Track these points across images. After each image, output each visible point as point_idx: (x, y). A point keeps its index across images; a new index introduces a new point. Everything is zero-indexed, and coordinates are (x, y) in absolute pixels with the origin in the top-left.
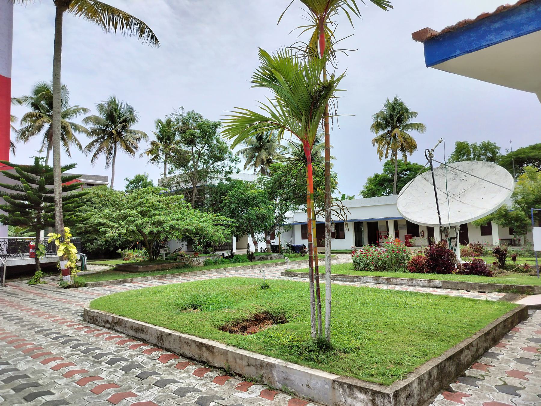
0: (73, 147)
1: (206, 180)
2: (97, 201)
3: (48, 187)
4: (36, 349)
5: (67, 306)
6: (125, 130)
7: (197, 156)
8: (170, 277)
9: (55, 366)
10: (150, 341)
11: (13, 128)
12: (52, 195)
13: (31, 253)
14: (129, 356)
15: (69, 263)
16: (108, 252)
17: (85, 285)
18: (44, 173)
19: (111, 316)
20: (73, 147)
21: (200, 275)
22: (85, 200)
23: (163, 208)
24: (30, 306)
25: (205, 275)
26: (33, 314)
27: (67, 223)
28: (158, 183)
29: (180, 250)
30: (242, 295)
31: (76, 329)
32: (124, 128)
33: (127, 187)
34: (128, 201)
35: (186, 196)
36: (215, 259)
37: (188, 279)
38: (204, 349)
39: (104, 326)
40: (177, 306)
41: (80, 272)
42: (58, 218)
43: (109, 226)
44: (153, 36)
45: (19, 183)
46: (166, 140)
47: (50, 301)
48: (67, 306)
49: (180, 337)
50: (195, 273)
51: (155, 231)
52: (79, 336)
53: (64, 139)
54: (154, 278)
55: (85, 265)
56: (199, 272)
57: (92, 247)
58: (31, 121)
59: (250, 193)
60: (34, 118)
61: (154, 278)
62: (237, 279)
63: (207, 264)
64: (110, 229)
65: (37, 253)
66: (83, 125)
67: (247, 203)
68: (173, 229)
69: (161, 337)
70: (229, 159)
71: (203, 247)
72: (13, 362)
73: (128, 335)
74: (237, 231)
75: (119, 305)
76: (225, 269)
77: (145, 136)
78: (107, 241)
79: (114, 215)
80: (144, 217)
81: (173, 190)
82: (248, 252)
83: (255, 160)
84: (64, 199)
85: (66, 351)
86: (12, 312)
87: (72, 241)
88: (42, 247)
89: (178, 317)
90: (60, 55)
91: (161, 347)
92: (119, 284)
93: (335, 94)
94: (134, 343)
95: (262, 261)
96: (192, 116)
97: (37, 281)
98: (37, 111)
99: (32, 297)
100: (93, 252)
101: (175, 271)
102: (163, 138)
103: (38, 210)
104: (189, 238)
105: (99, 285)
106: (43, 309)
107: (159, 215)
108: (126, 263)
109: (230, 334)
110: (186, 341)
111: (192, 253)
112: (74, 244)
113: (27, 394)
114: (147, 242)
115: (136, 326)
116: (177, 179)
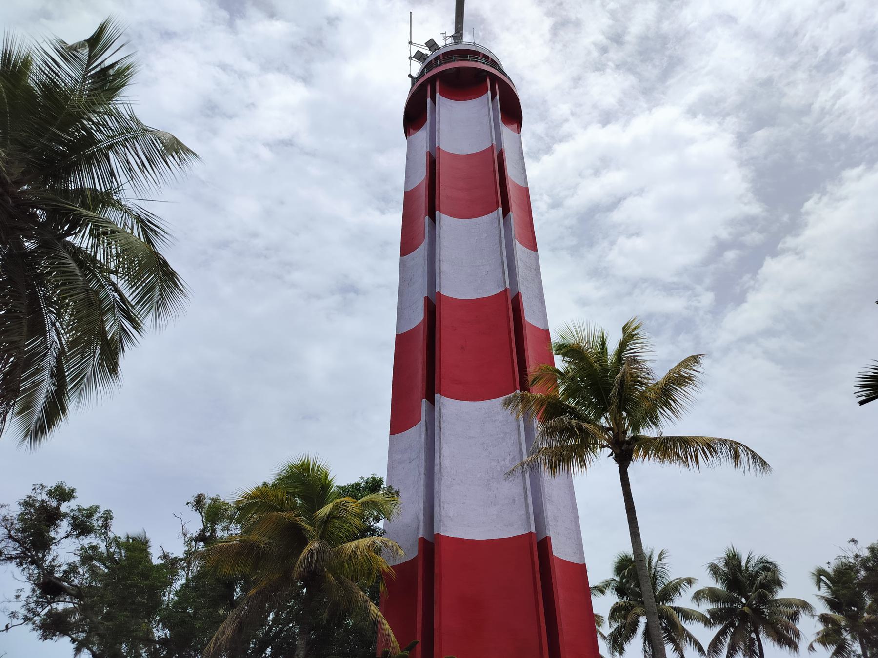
6: (764, 603)
11: (601, 634)
32: (763, 599)
44: (754, 455)
53: (672, 640)
77: (805, 606)
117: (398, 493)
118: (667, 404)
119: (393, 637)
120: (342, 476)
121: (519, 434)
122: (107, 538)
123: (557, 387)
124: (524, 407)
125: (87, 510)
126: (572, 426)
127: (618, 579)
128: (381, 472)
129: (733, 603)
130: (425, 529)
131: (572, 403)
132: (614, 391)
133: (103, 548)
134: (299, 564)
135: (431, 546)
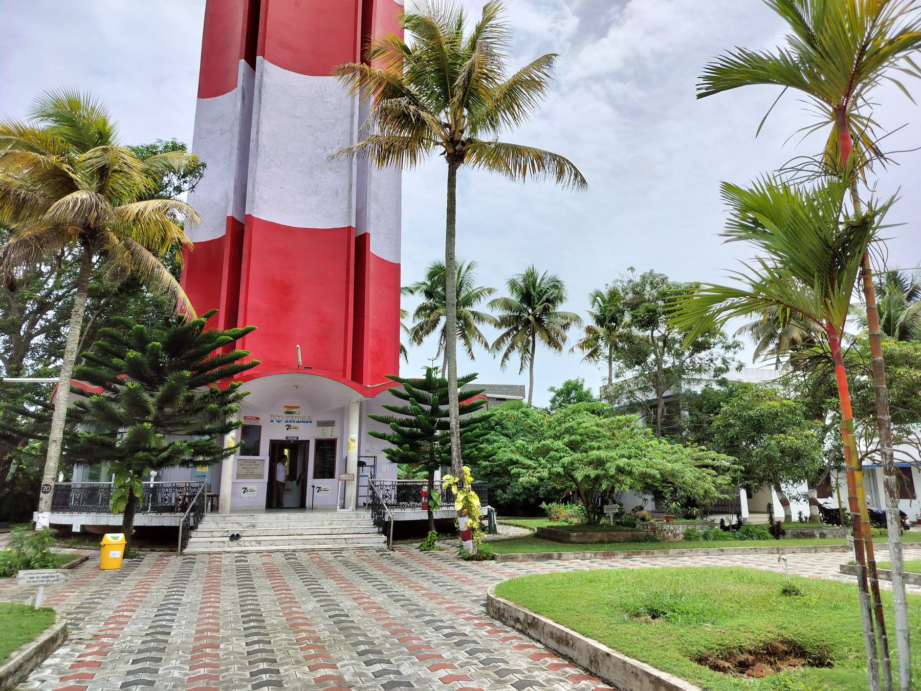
0: (477, 346)
1: (679, 386)
2: (510, 425)
3: (443, 408)
4: (424, 647)
5: (466, 587)
6: (546, 314)
7: (661, 344)
8: (622, 556)
10: (579, 662)
12: (447, 419)
15: (470, 521)
16: (526, 505)
17: (493, 558)
18: (438, 388)
20: (477, 346)
22: (493, 423)
23: (605, 436)
26: (423, 595)
27: (468, 460)
29: (641, 508)
30: (743, 602)
31: (475, 625)
32: (546, 310)
35: (646, 415)
36: (705, 530)
39: (513, 627)
41: (485, 536)
42: (455, 454)
43: (523, 465)
44: (577, 174)
45: (407, 404)
46: (610, 322)
47: (446, 578)
48: (466, 587)
49: (625, 663)
50: (665, 553)
51: (593, 476)
52: (479, 636)
53: (464, 336)
54: (595, 555)
56: (672, 551)
57: (505, 496)
59: (765, 406)
61: (595, 555)
62: (738, 571)
63: (688, 537)
64: (525, 471)
65: (431, 503)
67: (758, 426)
68: (622, 473)
69: (596, 658)
70: (720, 345)
72: (396, 660)
73: (547, 647)
74: (746, 479)
75: (536, 595)
76: (722, 551)
77: (577, 319)
79: (531, 448)
80: (575, 452)
81: (622, 404)
82: (771, 518)
83: (777, 341)
84: (462, 425)
85: (460, 657)
86: (400, 589)
87: (474, 487)
88: (435, 495)
89: (622, 628)
90: (454, 228)
91: (596, 674)
93: (880, 233)
94: (555, 661)
95: (800, 540)
96: (651, 280)
97: (431, 546)
99: (424, 569)
100: (507, 503)
101: (632, 546)
102: (605, 319)
103: (431, 441)
104: (659, 488)
105: (513, 559)
106: (436, 589)
107: (599, 448)
108: (552, 527)
109: (712, 672)
111: (661, 515)
114: (582, 493)
115: (558, 634)
117: (204, 165)
118: (510, 108)
119: (188, 304)
120: (128, 135)
121: (352, 123)
127: (429, 283)
128: (186, 137)
129: (521, 311)
131: (413, 88)
132: (459, 81)
135: (239, 229)
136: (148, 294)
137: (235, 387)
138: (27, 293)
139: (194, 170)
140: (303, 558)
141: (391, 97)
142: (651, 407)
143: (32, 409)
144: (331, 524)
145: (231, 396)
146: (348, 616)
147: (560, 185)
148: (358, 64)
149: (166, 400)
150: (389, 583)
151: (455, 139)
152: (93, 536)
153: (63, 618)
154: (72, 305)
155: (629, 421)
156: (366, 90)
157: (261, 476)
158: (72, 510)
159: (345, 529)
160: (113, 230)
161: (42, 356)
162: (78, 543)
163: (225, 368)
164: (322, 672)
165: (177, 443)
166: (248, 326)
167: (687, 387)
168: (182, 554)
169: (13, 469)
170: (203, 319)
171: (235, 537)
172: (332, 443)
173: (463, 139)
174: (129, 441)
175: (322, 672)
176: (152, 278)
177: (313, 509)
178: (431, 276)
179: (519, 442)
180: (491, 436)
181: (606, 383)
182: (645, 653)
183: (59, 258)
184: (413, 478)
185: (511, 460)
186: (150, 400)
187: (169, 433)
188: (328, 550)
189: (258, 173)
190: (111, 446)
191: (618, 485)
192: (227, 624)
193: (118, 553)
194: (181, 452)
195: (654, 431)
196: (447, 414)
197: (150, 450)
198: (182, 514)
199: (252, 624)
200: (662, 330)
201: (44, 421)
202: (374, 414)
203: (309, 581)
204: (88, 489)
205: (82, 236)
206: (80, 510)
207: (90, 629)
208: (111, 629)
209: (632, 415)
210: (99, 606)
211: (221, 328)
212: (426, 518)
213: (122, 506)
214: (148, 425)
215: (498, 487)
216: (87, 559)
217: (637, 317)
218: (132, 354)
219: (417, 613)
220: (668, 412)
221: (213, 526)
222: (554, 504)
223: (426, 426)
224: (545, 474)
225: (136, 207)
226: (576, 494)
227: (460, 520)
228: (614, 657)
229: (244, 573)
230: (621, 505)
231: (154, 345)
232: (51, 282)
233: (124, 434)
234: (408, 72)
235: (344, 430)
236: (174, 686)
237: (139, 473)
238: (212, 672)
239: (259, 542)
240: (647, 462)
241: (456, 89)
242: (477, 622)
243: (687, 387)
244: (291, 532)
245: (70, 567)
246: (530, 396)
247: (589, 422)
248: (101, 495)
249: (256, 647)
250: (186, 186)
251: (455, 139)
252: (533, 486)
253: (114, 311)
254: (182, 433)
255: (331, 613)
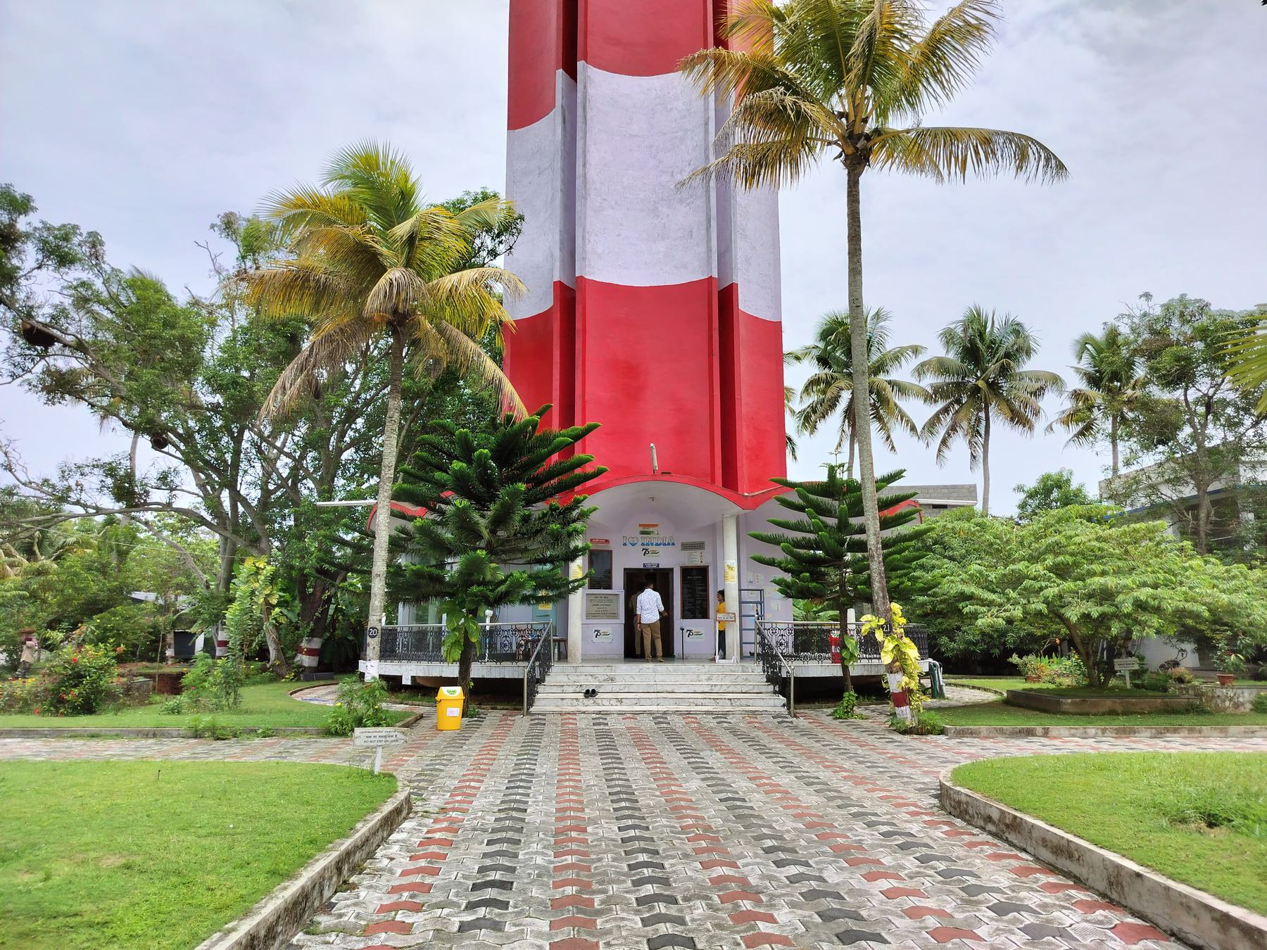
0: (899, 432)
1: (1236, 474)
2: (955, 543)
3: (855, 521)
4: (854, 848)
5: (907, 771)
7: (1201, 410)
9: (888, 890)
10: (1090, 883)
12: (863, 537)
13: (833, 655)
14: (1039, 906)
15: (905, 679)
16: (989, 659)
17: (942, 732)
18: (845, 494)
19: (997, 807)
20: (899, 432)
21: (1238, 737)
22: (930, 542)
23: (1112, 555)
24: (840, 761)
25: (1255, 740)
26: (845, 778)
27: (896, 594)
28: (1098, 492)
29: (1176, 664)
32: (1004, 371)
33: (1023, 506)
34: (1021, 543)
37: (1202, 745)
38: (1235, 932)
39: (983, 829)
40: (1161, 810)
41: (929, 701)
44: (1050, 156)
45: (802, 517)
46: (1111, 380)
47: (874, 757)
48: (907, 771)
49: (1168, 889)
50: (1221, 731)
51: (1095, 615)
53: (879, 418)
54: (1104, 731)
55: (941, 687)
56: (1233, 729)
57: (953, 645)
58: (818, 391)
60: (822, 386)
61: (1104, 731)
64: (985, 609)
65: (844, 654)
66: (914, 381)
69: (1116, 877)
71: (1248, 661)
72: (816, 863)
73: (1037, 859)
77: (1056, 380)
78: (983, 634)
79: (992, 576)
80: (1064, 579)
81: (1139, 506)
84: (886, 545)
85: (908, 864)
86: (810, 768)
87: (908, 633)
88: (852, 643)
89: (1163, 838)
90: (859, 261)
92: (1017, 738)
94: (1052, 879)
96: (1182, 310)
97: (848, 713)
98: (827, 370)
101: (1162, 719)
102: (1101, 379)
103: (839, 567)
104: (1205, 633)
105: (972, 734)
106: (862, 771)
107: (1104, 573)
108: (1031, 690)
110: (1184, 900)
111: (1212, 674)
112: (913, 640)
113: (842, 930)
114: (1077, 640)
115: (1055, 841)
116: (1149, 477)
117: (522, 218)
120: (433, 190)
121: (706, 132)
122: (101, 272)
123: (770, 43)
124: (716, 74)
125: (59, 229)
126: (785, 107)
127: (821, 345)
128: (498, 185)
130: (563, 268)
131: (789, 69)
132: (856, 47)
133: (98, 284)
134: (374, 301)
135: (569, 296)
136: (467, 391)
137: (578, 502)
138: (333, 399)
139: (509, 227)
140: (678, 722)
141: (760, 90)
142: (1188, 509)
143: (348, 538)
144: (709, 679)
145: (575, 513)
146: (744, 800)
147: (1022, 176)
148: (711, 50)
149: (499, 521)
150: (796, 760)
151: (856, 132)
152: (426, 689)
153: (405, 786)
154: (384, 409)
155: (1152, 531)
156: (724, 84)
157: (614, 616)
158: (400, 658)
159: (729, 686)
160: (424, 313)
161: (353, 475)
162: (409, 698)
163: (564, 478)
164: (719, 871)
165: (516, 574)
166: (589, 423)
167: (1250, 474)
168: (528, 713)
169: (333, 607)
170: (536, 418)
171: (590, 694)
172: (703, 572)
173: (867, 131)
174: (460, 573)
175: (719, 871)
176: (475, 369)
177: (683, 659)
178: (824, 335)
179: (974, 568)
180: (928, 560)
181: (1110, 475)
182: (1200, 877)
183: (364, 354)
184: (815, 619)
185: (962, 594)
186: (482, 522)
187: (505, 562)
188: (707, 713)
189: (588, 220)
190: (439, 580)
191: (1138, 628)
192: (591, 802)
193: (456, 711)
194: (521, 585)
195: (1195, 546)
196: (862, 530)
197: (484, 583)
198: (525, 664)
199: (623, 804)
200: (1203, 386)
201: (363, 552)
202: (757, 532)
203: (688, 753)
204: (418, 632)
205: (389, 323)
206: (408, 658)
207: (435, 802)
208: (458, 802)
209: (1158, 522)
210: (442, 774)
211: (555, 428)
212: (840, 674)
213: (457, 654)
214: (482, 553)
215: (941, 633)
216: (421, 717)
217: (1157, 370)
218: (457, 465)
219: (840, 802)
220: (1215, 515)
221: (563, 679)
222: (1031, 657)
223: (829, 547)
224: (1018, 613)
225: (450, 280)
226: (1065, 643)
227: (890, 677)
228: (1149, 879)
229: (606, 740)
230: (1141, 658)
231: (481, 454)
232: (358, 383)
233: (454, 566)
234: (782, 47)
235: (717, 552)
236: (539, 875)
237: (474, 612)
238: (580, 861)
239: (620, 701)
240: (1185, 593)
241: (852, 60)
242: (927, 818)
243: (1250, 474)
244: (659, 689)
245: (404, 726)
246: (986, 500)
247: (1085, 534)
248: (430, 639)
249: (632, 833)
250: (502, 248)
251: (856, 132)
252: (997, 630)
253: (431, 413)
254: (522, 561)
255: (723, 796)
